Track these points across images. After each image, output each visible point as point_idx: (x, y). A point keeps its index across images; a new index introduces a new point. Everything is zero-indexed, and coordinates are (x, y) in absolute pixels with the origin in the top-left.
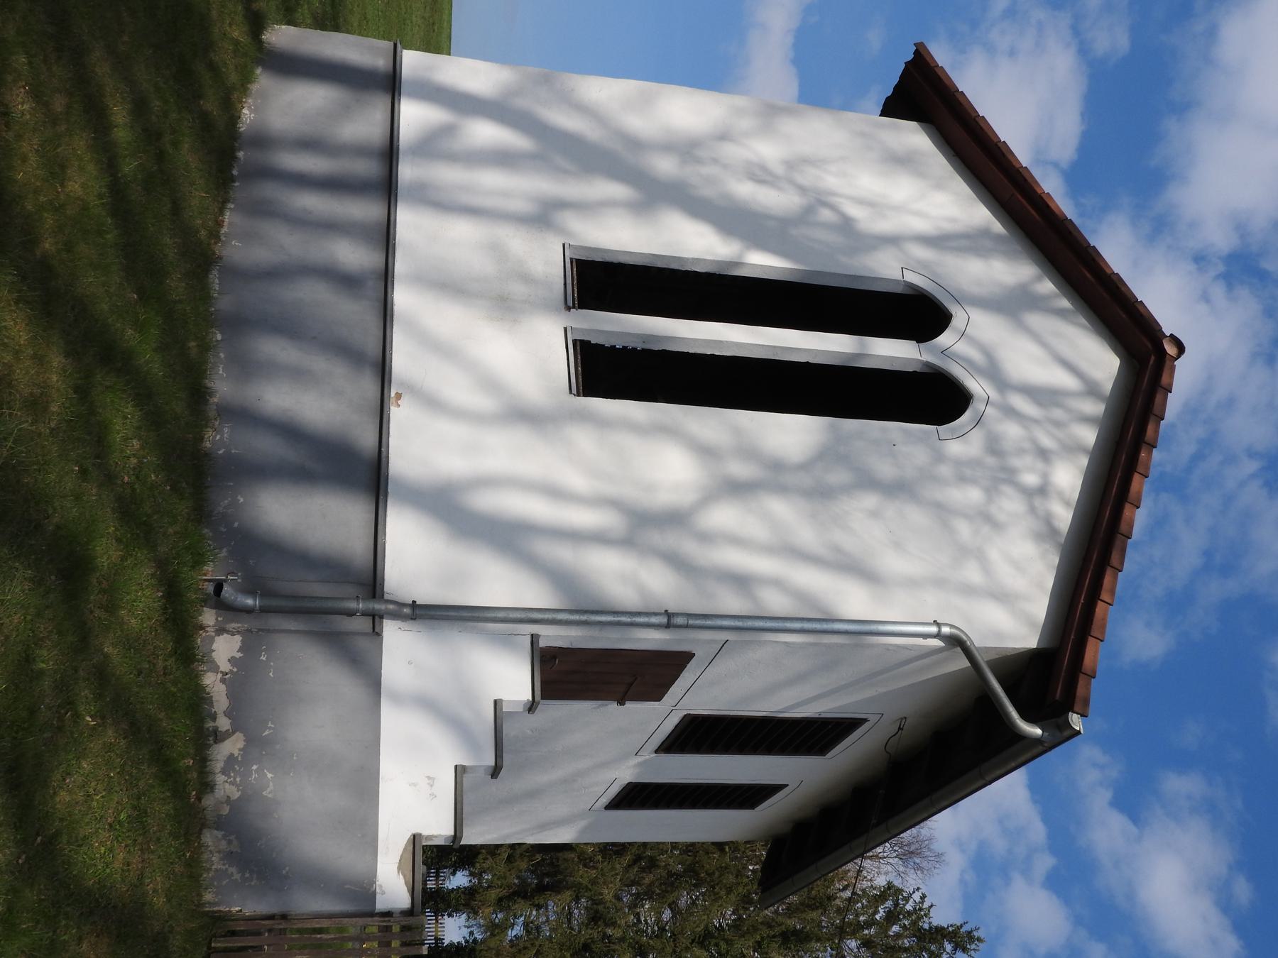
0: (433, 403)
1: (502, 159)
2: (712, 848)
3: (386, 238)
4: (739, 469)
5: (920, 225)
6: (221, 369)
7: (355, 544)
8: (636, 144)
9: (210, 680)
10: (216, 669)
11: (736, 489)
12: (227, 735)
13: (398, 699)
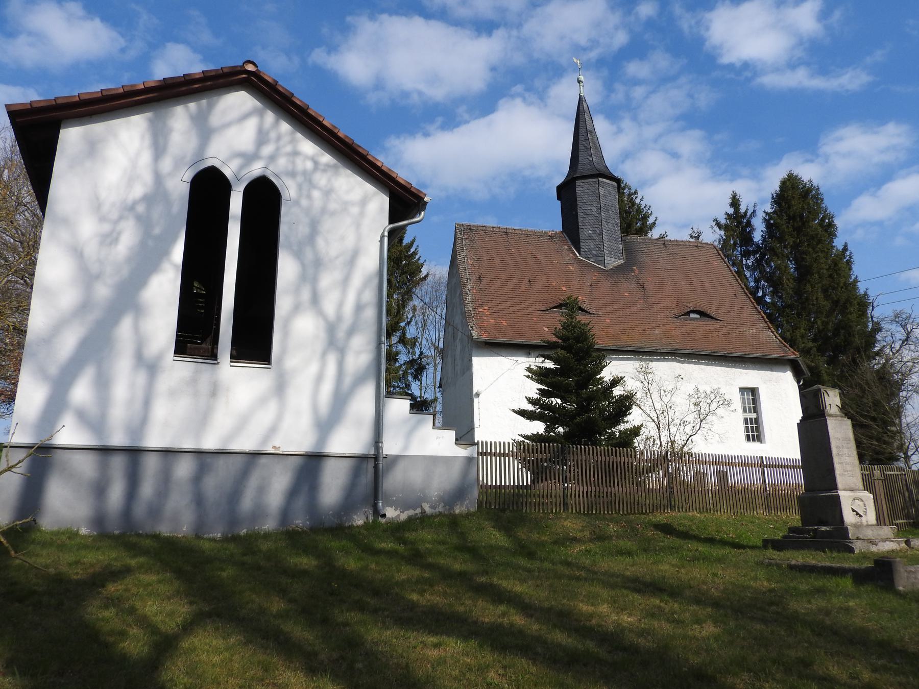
0: (273, 430)
1: (103, 384)
2: (29, 303)
3: (168, 453)
4: (306, 295)
5: (146, 157)
6: (264, 527)
7: (345, 465)
8: (84, 307)
9: (404, 517)
10: (399, 515)
11: (315, 300)
12: (422, 508)
13: (406, 447)
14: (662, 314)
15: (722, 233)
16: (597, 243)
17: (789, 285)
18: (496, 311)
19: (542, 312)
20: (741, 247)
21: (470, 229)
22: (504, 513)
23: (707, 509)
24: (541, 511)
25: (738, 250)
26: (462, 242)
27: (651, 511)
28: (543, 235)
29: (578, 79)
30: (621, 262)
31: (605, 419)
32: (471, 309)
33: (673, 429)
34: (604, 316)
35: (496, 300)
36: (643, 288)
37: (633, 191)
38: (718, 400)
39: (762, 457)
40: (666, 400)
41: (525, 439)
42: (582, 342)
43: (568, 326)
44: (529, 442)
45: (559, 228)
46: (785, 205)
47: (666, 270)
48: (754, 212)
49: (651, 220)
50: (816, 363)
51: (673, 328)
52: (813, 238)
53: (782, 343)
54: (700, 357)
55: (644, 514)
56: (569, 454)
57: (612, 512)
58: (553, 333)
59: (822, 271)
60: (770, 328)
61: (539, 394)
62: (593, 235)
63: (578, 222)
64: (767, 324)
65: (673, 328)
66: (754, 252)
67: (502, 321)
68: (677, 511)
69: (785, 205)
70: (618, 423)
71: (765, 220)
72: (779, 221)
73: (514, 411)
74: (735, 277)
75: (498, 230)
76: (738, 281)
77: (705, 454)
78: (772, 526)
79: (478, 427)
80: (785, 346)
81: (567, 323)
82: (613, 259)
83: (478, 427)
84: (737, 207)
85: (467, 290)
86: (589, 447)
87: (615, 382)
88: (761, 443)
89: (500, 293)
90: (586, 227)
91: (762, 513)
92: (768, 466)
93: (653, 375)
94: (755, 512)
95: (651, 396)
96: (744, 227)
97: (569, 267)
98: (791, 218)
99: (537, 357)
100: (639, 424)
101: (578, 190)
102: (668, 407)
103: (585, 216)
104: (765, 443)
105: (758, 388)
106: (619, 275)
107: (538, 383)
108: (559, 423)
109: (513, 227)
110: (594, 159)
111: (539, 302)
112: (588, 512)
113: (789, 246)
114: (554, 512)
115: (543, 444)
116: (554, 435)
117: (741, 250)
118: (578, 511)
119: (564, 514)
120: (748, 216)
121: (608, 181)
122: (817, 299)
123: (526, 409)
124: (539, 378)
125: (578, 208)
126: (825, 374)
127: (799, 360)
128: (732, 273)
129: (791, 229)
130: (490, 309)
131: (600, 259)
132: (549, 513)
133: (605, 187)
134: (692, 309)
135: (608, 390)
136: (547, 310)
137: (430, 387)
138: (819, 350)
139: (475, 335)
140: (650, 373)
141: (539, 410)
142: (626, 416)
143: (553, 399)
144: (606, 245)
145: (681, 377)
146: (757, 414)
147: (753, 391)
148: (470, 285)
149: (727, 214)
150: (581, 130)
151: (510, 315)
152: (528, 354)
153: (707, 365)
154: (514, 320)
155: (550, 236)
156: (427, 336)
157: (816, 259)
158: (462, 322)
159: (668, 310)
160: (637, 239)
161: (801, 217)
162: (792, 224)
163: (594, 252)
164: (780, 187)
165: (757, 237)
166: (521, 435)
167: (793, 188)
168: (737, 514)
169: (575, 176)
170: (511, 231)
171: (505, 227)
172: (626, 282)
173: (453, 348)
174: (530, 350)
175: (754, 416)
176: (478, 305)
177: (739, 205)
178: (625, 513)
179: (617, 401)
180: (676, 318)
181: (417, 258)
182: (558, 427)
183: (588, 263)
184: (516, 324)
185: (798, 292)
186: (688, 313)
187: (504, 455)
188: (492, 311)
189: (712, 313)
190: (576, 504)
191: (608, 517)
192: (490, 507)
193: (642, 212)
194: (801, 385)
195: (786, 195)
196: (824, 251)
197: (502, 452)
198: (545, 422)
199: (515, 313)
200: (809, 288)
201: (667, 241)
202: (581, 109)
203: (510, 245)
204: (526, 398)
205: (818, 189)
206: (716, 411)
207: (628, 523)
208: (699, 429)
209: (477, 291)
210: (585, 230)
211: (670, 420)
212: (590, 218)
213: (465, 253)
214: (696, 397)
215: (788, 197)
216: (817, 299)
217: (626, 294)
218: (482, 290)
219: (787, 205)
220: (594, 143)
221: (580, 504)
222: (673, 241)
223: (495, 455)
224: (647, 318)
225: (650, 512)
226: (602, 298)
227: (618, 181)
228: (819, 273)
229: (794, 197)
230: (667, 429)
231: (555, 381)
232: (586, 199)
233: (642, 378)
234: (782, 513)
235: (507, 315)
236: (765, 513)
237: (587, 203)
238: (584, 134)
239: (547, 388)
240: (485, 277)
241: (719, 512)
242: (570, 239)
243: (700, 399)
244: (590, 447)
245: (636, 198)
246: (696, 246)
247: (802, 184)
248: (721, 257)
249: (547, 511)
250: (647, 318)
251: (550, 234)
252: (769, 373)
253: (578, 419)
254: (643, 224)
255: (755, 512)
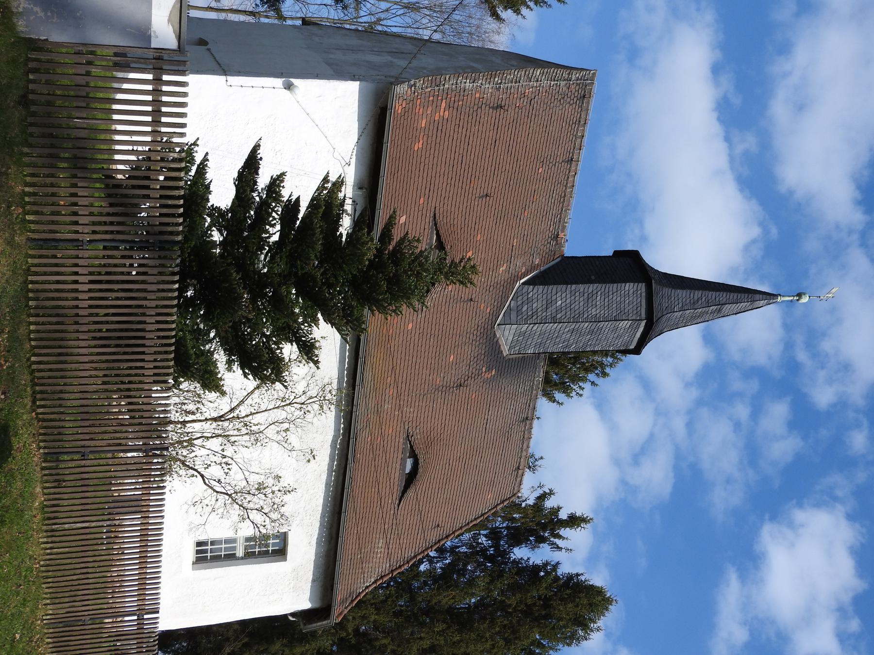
14: (415, 415)
15: (531, 502)
16: (539, 314)
17: (445, 599)
18: (439, 131)
19: (432, 215)
20: (507, 528)
21: (584, 96)
22: (19, 103)
23: (49, 519)
24: (27, 189)
25: (503, 523)
26: (564, 80)
27: (40, 416)
28: (560, 222)
29: (804, 294)
30: (506, 352)
31: (236, 327)
32: (446, 86)
33: (215, 444)
34: (419, 320)
35: (460, 133)
36: (461, 385)
37: (607, 370)
38: (269, 527)
39: (158, 612)
40: (271, 432)
41: (199, 166)
42: (389, 290)
43: (421, 265)
44: (193, 173)
45: (570, 250)
46: (566, 594)
47: (485, 421)
48: (559, 548)
49: (559, 396)
50: (320, 636)
51: (390, 432)
52: (514, 632)
53: (356, 597)
54: (342, 471)
55: (34, 402)
56: (160, 257)
57: (35, 340)
58: (407, 233)
59: (464, 646)
60: (382, 577)
61: (289, 201)
62: (554, 307)
63: (577, 283)
64: (388, 574)
65: (390, 432)
66: (496, 546)
67: (421, 142)
68: (44, 465)
69: (566, 594)
70: (229, 352)
71: (546, 564)
72: (544, 585)
73: (256, 147)
74: (465, 525)
75: (577, 146)
76: (459, 529)
77: (162, 517)
78: (18, 636)
79: (229, 83)
80: (352, 601)
81: (427, 261)
82: (511, 338)
83: (229, 83)
84: (568, 524)
85: (480, 82)
86: (174, 298)
87: (308, 350)
88: (193, 564)
89: (470, 143)
90: (568, 296)
91: (45, 612)
92: (141, 622)
93: (318, 412)
94: (48, 601)
95: (278, 407)
96: (538, 533)
97: (505, 265)
98: (546, 602)
99: (353, 201)
100: (225, 388)
101: (629, 287)
102: (256, 436)
103: (586, 295)
104: (193, 570)
105: (286, 560)
106: (484, 346)
107: (313, 200)
108: (230, 237)
109: (579, 173)
110: (676, 314)
111: (449, 211)
112: (32, 291)
113: (504, 598)
114: (28, 217)
115: (182, 202)
116: (207, 224)
117: (502, 528)
118: (33, 269)
119: (23, 238)
120: (552, 539)
121: (638, 335)
122: (421, 638)
123: (260, 171)
124: (323, 203)
125: (600, 285)
126: (303, 649)
127: (329, 621)
128: (472, 521)
129: (529, 602)
130: (445, 121)
131: (513, 315)
132: (23, 208)
133: (630, 330)
134: (421, 461)
135: (294, 334)
136: (436, 224)
137: (304, 10)
138: (342, 640)
139: (401, 89)
140: (321, 407)
141: (257, 199)
142: (242, 368)
143: (278, 227)
144: (535, 328)
145: (312, 459)
146: (242, 558)
147: (281, 553)
148: (488, 87)
149: (559, 508)
150: (724, 295)
151: (432, 156)
152: (359, 186)
153: (327, 484)
154: (422, 164)
155: (558, 235)
156: (394, 11)
157: (482, 637)
158: (424, 68)
159: (422, 424)
160: (538, 376)
161: (547, 617)
162: (537, 604)
163: (525, 308)
164: (592, 586)
165: (520, 553)
166: (205, 159)
167: (591, 605)
168: (43, 572)
169: (653, 281)
170: (573, 168)
171: (582, 158)
172: (473, 358)
173: (376, 50)
174: (366, 189)
175: (240, 553)
176: (453, 99)
177: (571, 527)
178: (34, 367)
179: (272, 351)
180: (408, 436)
181: (529, 3)
182: (222, 235)
183: (508, 297)
184: (414, 167)
185: (430, 611)
186: (414, 455)
187: (157, 113)
188: (440, 125)
189: (411, 493)
190: (56, 265)
191: (21, 331)
192: (35, 71)
193: (573, 383)
194: (288, 618)
195: (581, 595)
196: (494, 648)
197: (164, 109)
198: (233, 208)
199: (435, 166)
200: (439, 627)
201: (531, 424)
202: (757, 296)
203: (551, 165)
204: (283, 174)
205: (586, 639)
206: (248, 522)
207: (8, 374)
208: (214, 491)
209: (477, 100)
210: (564, 295)
211: (233, 439)
212: (582, 304)
213: (545, 83)
214: (275, 489)
215: (579, 598)
216: (421, 638)
217: (452, 357)
218: (479, 110)
219: (566, 596)
220: (701, 315)
221: (58, 274)
222: (530, 433)
223: (157, 92)
224: (411, 390)
225: (37, 414)
226: (449, 319)
227: (637, 351)
228: (461, 641)
229: (577, 606)
230: (216, 432)
231: (314, 234)
232: (614, 298)
233: (313, 392)
234: (51, 646)
235: (432, 153)
236: (48, 617)
237: (606, 300)
238: (717, 299)
239: (300, 216)
240: (501, 117)
241: (45, 540)
242: (549, 268)
243: (270, 496)
244: (175, 302)
245: (597, 375)
246: (518, 468)
247: (595, 617)
248: (498, 505)
249: (29, 203)
250: (411, 390)
251: (561, 235)
252: (310, 576)
253: (236, 276)
254: (556, 384)
255: (48, 601)
